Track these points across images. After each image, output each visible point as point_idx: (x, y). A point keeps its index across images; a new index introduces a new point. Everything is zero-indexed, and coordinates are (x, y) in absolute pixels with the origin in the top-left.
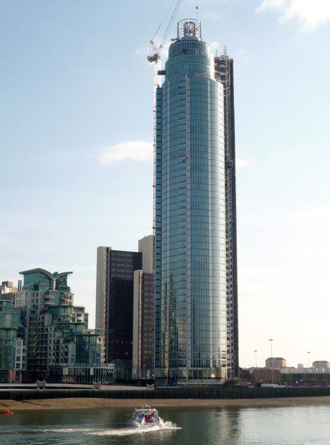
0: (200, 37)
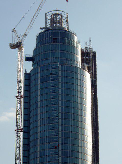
0: (68, 28)
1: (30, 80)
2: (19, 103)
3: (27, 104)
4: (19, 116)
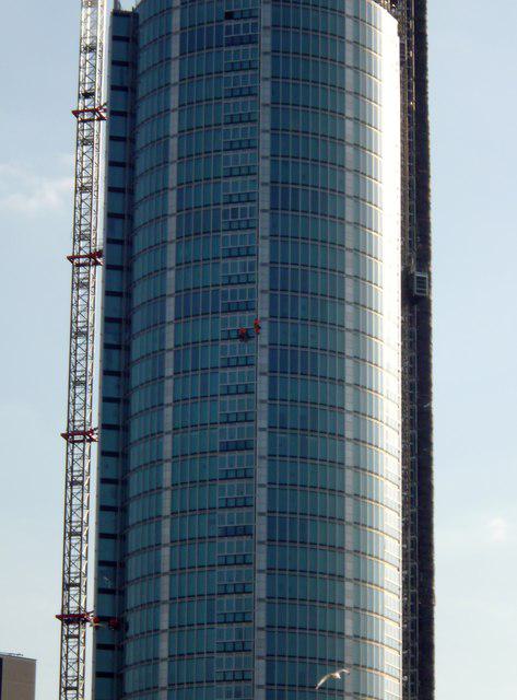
1: (136, 41)
2: (86, 142)
3: (108, 680)
4: (84, 196)
